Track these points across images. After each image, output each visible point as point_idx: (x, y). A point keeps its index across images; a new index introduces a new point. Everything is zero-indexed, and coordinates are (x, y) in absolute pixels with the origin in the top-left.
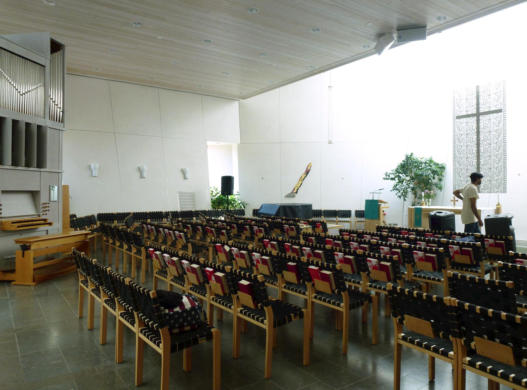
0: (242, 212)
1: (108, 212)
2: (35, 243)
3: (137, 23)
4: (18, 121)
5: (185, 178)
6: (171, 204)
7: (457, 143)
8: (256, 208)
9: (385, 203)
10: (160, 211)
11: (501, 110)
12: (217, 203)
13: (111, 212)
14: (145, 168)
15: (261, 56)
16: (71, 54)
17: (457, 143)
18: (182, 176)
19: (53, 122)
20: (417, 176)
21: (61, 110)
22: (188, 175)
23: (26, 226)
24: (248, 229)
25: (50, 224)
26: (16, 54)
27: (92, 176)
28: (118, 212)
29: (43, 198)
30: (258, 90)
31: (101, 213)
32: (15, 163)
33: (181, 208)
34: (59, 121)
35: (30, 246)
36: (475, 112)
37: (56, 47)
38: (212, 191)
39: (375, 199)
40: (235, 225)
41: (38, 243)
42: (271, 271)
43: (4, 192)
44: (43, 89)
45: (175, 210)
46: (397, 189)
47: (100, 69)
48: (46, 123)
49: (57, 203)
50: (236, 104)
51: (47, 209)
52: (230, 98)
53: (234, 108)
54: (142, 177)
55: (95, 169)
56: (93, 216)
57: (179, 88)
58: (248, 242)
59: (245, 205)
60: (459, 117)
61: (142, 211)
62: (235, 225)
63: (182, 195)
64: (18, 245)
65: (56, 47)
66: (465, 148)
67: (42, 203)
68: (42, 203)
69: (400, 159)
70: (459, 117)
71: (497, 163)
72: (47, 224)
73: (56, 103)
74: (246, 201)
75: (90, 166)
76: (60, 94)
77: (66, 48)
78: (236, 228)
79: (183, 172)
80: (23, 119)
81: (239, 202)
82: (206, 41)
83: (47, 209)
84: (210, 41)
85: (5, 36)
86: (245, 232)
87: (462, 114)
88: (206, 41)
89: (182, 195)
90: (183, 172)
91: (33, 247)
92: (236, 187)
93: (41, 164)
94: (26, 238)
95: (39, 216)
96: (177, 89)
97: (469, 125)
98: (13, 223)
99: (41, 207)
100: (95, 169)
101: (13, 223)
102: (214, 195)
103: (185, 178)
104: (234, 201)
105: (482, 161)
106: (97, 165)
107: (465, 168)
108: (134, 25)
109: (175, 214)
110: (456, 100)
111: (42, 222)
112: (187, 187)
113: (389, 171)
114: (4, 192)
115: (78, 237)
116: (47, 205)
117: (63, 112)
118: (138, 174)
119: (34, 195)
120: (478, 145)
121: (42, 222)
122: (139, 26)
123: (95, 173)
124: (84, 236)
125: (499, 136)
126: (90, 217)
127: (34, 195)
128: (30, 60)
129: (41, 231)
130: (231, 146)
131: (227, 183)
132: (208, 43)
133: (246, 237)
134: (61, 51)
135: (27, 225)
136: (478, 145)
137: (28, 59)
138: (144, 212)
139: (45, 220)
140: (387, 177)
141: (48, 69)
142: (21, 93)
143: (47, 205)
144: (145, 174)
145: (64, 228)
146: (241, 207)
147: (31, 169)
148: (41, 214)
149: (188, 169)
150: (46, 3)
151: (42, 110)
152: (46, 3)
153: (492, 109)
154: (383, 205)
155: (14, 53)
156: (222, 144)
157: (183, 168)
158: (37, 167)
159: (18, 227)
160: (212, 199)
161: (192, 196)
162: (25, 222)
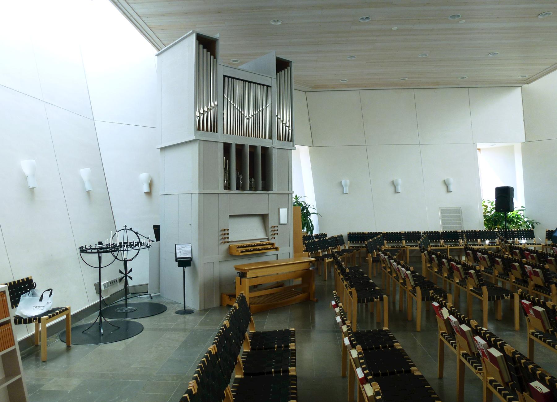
0: (529, 234)
1: (359, 232)
2: (250, 271)
3: (365, 17)
4: (244, 145)
5: (448, 191)
6: (430, 222)
8: (551, 229)
10: (417, 231)
12: (490, 221)
13: (362, 232)
14: (400, 181)
15: (540, 17)
16: (297, 70)
18: (444, 188)
19: (281, 142)
21: (290, 128)
22: (452, 188)
23: (251, 251)
24: (518, 268)
25: (276, 249)
26: (242, 80)
27: (343, 193)
28: (370, 232)
29: (272, 222)
30: (546, 67)
31: (351, 232)
32: (238, 188)
33: (443, 227)
34: (288, 141)
35: (246, 273)
37: (282, 65)
38: (486, 206)
40: (499, 260)
41: (254, 271)
42: (507, 380)
43: (231, 216)
44: (270, 109)
45: (436, 231)
47: (347, 80)
48: (273, 143)
50: (517, 92)
51: (276, 232)
52: (507, 85)
53: (514, 97)
54: (396, 192)
55: (346, 186)
56: (341, 237)
57: (438, 85)
58: (517, 285)
59: (535, 225)
61: (396, 231)
62: (499, 260)
63: (444, 211)
64: (236, 272)
65: (282, 65)
67: (270, 226)
68: (270, 226)
72: (274, 248)
73: (284, 122)
74: (535, 217)
75: (341, 182)
76: (289, 113)
77: (293, 65)
78: (501, 264)
79: (446, 184)
80: (247, 142)
81: (526, 220)
82: (453, 16)
83: (276, 232)
84: (459, 16)
85: (240, 67)
86: (513, 271)
88: (453, 16)
89: (444, 211)
90: (446, 184)
91: (249, 275)
92: (519, 202)
93: (267, 187)
94: (241, 265)
95: (268, 239)
96: (435, 86)
98: (238, 247)
99: (270, 230)
100: (346, 186)
101: (238, 247)
102: (489, 210)
103: (448, 191)
104: (518, 218)
106: (348, 182)
108: (361, 21)
109: (434, 236)
111: (270, 246)
112: (449, 201)
114: (231, 216)
115: (304, 264)
116: (276, 228)
117: (292, 130)
118: (392, 189)
119: (264, 217)
121: (270, 246)
122: (367, 21)
123: (346, 190)
124: (308, 263)
126: (336, 238)
127: (264, 217)
128: (258, 84)
129: (270, 256)
130: (512, 147)
131: (504, 196)
132: (457, 19)
133: (516, 279)
134: (289, 68)
135: (252, 250)
137: (254, 83)
138: (398, 231)
139: (272, 244)
141: (274, 89)
142: (248, 117)
143: (276, 228)
144: (400, 189)
145: (296, 251)
146: (528, 227)
147: (258, 192)
148: (270, 238)
149: (451, 180)
150: (273, 23)
151: (270, 132)
152: (273, 23)
155: (239, 79)
156: (498, 145)
157: (445, 179)
158: (262, 190)
159: (242, 252)
160: (485, 216)
161: (458, 213)
162: (251, 246)
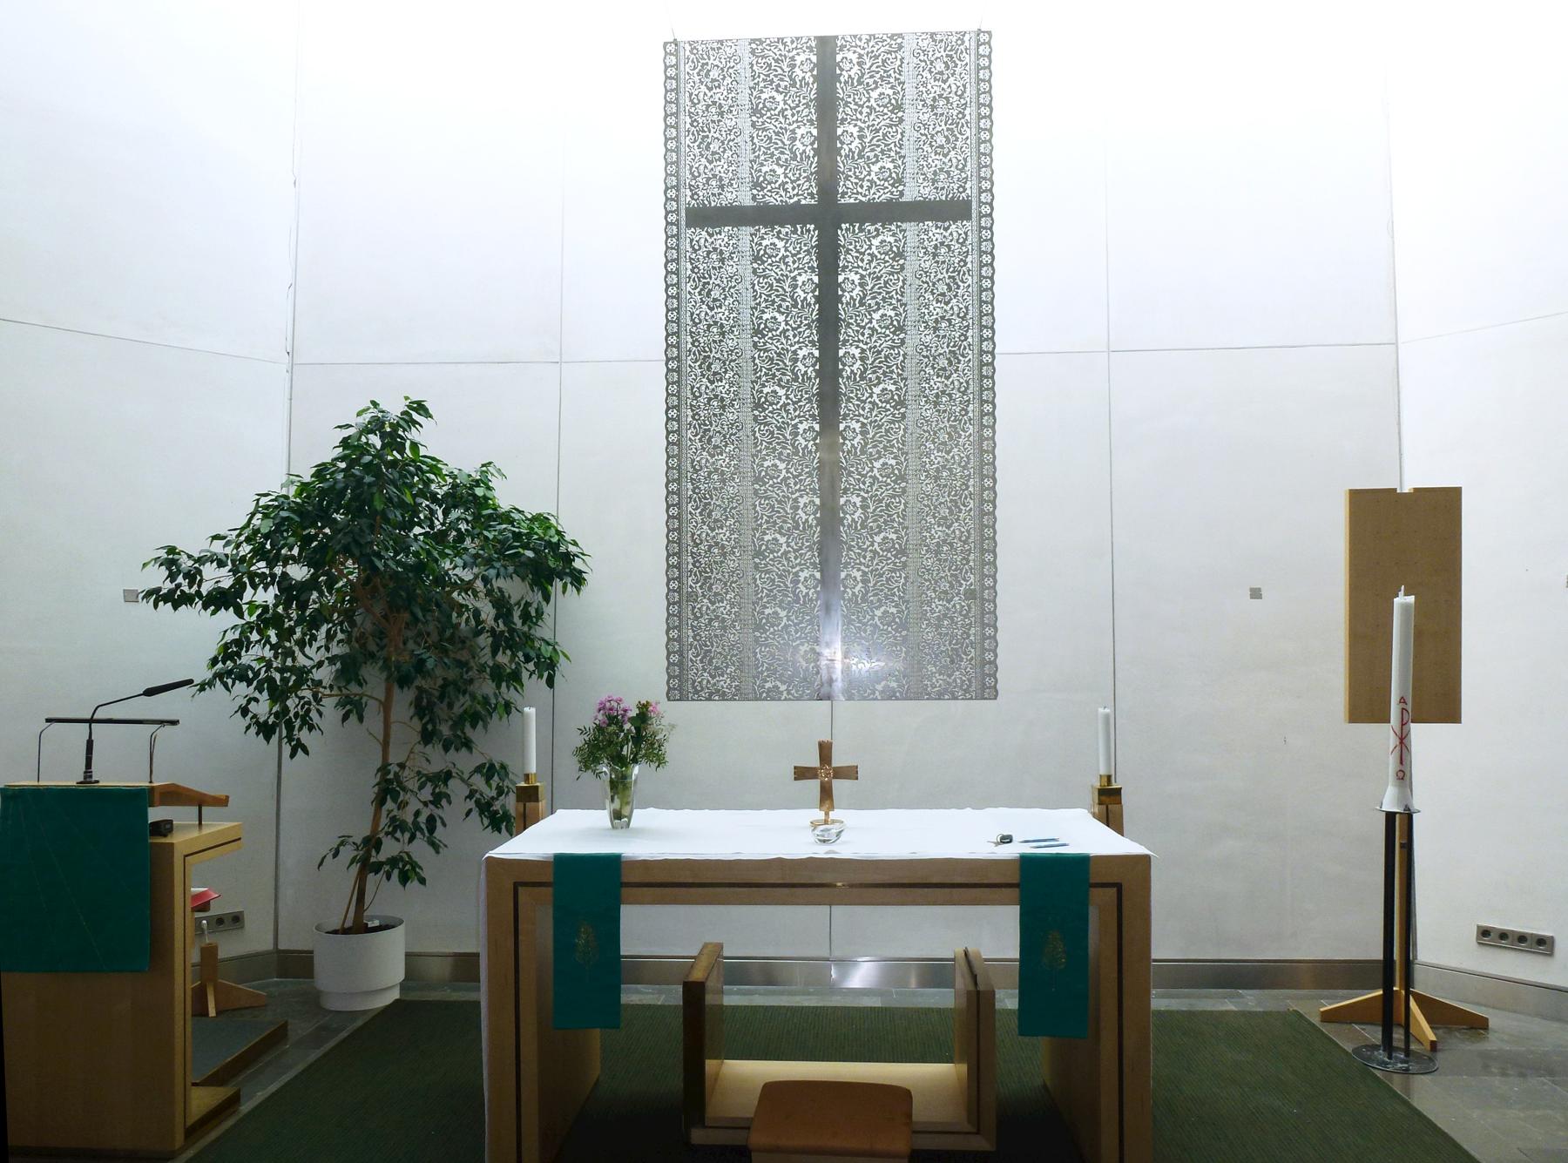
7: (694, 374)
9: (200, 801)
11: (967, 204)
17: (694, 374)
20: (390, 581)
36: (804, 193)
39: (109, 776)
46: (242, 675)
49: (190, 1080)
60: (703, 217)
66: (749, 487)
69: (272, 450)
70: (703, 217)
71: (944, 522)
87: (728, 198)
97: (775, 421)
105: (850, 352)
107: (746, 540)
110: (685, 100)
113: (193, 544)
120: (829, 326)
125: (953, 358)
136: (829, 326)
140: (179, 585)
153: (913, 192)
154: (187, 831)
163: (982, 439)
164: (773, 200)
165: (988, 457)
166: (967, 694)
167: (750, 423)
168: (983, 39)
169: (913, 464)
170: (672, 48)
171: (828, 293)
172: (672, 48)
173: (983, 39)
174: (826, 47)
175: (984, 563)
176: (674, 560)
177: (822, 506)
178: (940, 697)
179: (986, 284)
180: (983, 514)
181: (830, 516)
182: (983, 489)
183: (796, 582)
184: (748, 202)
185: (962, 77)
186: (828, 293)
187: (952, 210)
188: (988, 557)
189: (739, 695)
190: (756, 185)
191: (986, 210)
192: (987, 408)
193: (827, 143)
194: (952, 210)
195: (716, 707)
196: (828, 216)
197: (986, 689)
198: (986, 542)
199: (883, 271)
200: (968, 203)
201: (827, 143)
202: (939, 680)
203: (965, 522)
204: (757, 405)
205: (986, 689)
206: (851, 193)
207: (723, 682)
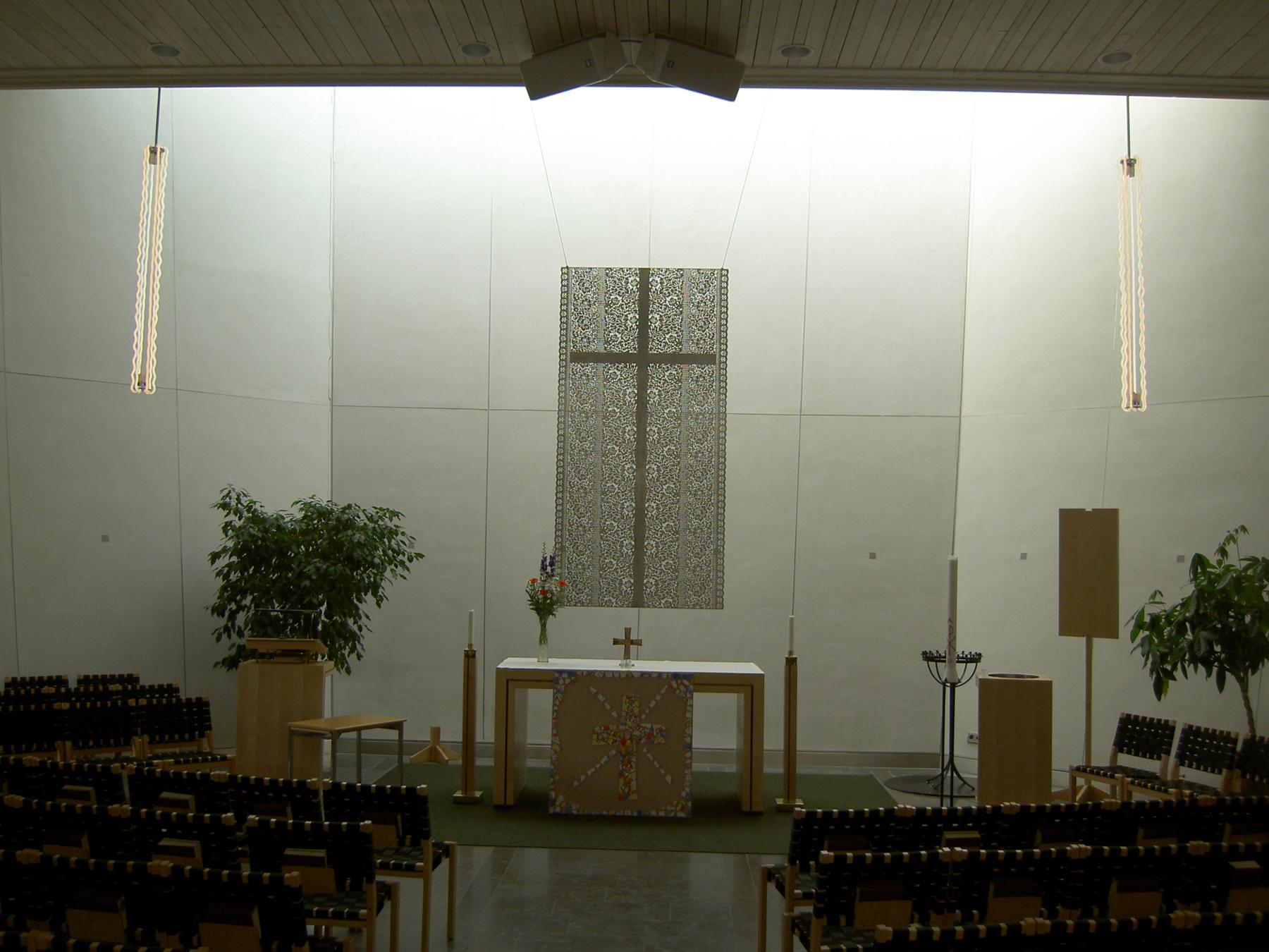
60: (579, 357)
70: (579, 357)
87: (592, 347)
120: (641, 455)
136: (641, 455)
163: (719, 476)
164: (616, 350)
165: (721, 473)
166: (708, 606)
167: (598, 540)
168: (724, 273)
169: (684, 449)
170: (566, 271)
171: (642, 400)
172: (566, 271)
173: (724, 273)
174: (644, 273)
175: (720, 425)
176: (560, 495)
177: (635, 546)
178: (694, 607)
179: (721, 511)
180: (717, 590)
181: (640, 513)
182: (720, 425)
183: (622, 546)
184: (603, 351)
185: (713, 291)
186: (642, 400)
187: (709, 359)
188: (720, 574)
189: (590, 603)
190: (607, 342)
191: (723, 359)
192: (723, 384)
193: (643, 323)
194: (709, 359)
195: (579, 609)
196: (642, 358)
197: (718, 604)
198: (720, 529)
199: (671, 313)
200: (714, 356)
201: (643, 323)
202: (694, 599)
203: (710, 442)
204: (603, 531)
205: (718, 604)
206: (655, 348)
207: (583, 597)
